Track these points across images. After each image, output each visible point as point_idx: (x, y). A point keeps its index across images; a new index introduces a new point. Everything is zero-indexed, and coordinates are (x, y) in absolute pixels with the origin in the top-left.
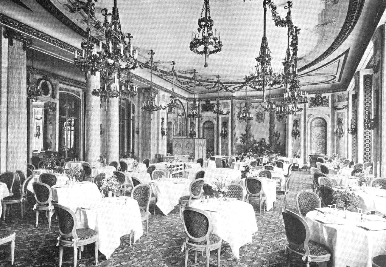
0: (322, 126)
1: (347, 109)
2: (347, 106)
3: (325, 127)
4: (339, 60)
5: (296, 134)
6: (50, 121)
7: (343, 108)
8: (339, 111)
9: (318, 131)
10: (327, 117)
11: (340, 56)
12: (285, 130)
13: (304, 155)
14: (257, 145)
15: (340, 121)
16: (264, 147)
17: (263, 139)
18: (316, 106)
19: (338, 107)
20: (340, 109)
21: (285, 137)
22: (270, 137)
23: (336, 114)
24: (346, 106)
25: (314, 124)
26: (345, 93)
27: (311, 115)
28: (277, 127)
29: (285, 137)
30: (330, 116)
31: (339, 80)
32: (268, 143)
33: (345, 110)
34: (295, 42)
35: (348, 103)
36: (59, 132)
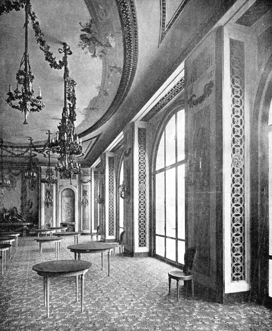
0: (71, 197)
1: (90, 183)
2: (91, 181)
3: (116, 239)
4: (91, 141)
5: (48, 204)
6: (202, 144)
7: (88, 182)
8: (85, 184)
9: (66, 200)
10: (74, 188)
11: (91, 139)
12: (39, 198)
13: (56, 219)
14: (7, 214)
15: (85, 192)
16: (16, 216)
17: (15, 208)
18: (66, 178)
19: (84, 181)
20: (85, 183)
21: (38, 207)
22: (21, 206)
23: (82, 187)
24: (90, 180)
25: (64, 194)
26: (89, 169)
27: (62, 186)
28: (30, 196)
29: (38, 208)
30: (77, 187)
31: (85, 158)
32: (19, 212)
33: (89, 184)
34: (126, 29)
35: (91, 178)
36: (114, 138)
